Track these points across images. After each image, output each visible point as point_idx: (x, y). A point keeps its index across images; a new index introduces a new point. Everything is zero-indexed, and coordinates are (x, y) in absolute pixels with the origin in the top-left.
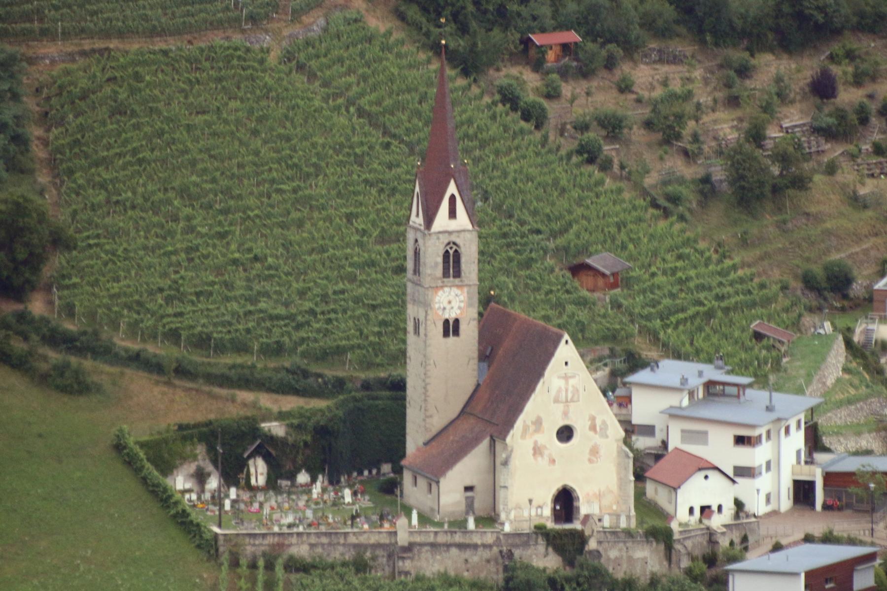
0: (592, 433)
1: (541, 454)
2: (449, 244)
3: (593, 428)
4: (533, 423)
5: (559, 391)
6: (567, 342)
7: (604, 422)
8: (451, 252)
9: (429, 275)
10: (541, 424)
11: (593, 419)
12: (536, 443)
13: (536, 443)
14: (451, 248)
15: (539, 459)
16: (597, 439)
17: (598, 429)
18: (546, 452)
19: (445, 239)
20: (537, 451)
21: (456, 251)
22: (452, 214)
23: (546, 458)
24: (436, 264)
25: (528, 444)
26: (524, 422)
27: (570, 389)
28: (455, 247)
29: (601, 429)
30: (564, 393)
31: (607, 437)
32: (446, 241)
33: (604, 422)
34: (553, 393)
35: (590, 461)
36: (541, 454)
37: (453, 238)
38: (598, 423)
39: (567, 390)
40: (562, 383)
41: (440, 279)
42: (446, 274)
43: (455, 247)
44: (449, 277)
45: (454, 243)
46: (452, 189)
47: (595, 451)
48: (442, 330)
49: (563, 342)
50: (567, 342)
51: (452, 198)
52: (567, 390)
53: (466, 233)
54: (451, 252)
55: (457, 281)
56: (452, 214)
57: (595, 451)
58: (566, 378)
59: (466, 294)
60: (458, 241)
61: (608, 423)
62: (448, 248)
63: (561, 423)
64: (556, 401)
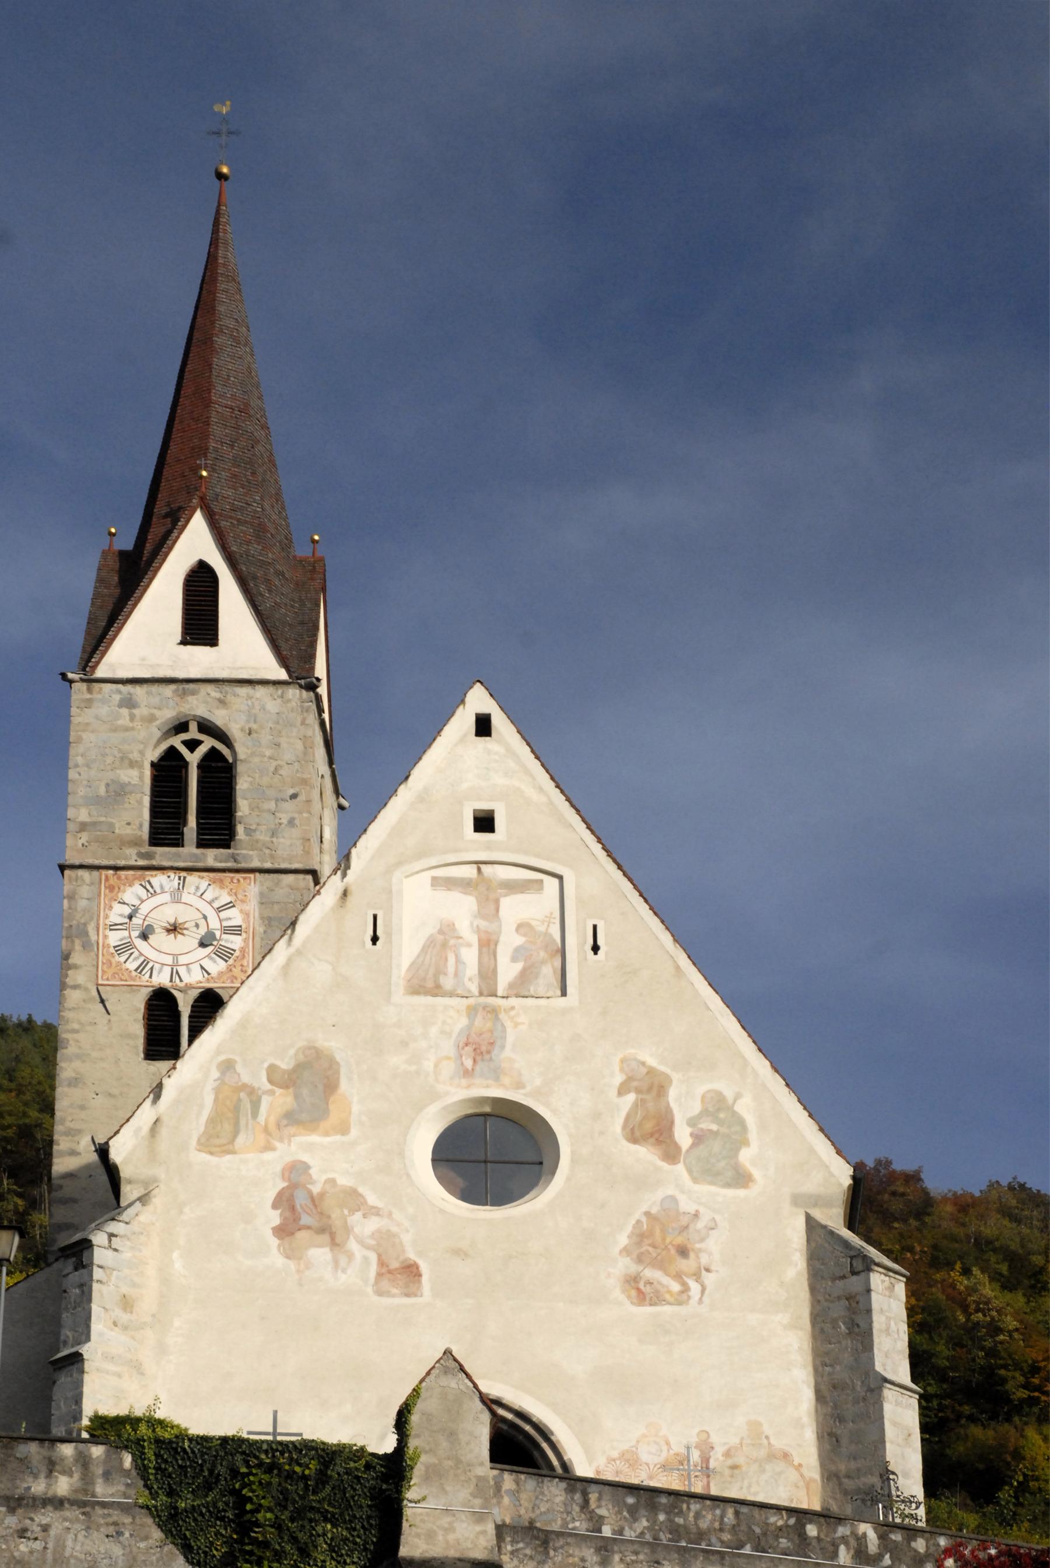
0: (645, 1154)
1: (331, 1235)
2: (182, 727)
3: (653, 1129)
4: (279, 1079)
5: (443, 941)
6: (483, 726)
7: (717, 1106)
8: (193, 759)
9: (83, 827)
10: (331, 1086)
11: (651, 1087)
12: (296, 1173)
13: (296, 1173)
14: (192, 745)
15: (320, 1254)
16: (681, 1187)
17: (683, 1136)
18: (364, 1227)
19: (167, 707)
20: (303, 1214)
21: (213, 754)
22: (200, 624)
23: (360, 1265)
24: (119, 792)
25: (254, 1173)
26: (228, 1066)
27: (509, 941)
28: (208, 743)
29: (698, 1138)
30: (470, 956)
31: (742, 1179)
32: (168, 714)
33: (717, 1106)
34: (407, 946)
35: (640, 1292)
36: (331, 1235)
37: (200, 705)
38: (684, 1105)
39: (488, 945)
40: (461, 909)
41: (135, 843)
42: (165, 829)
43: (208, 743)
44: (178, 842)
45: (207, 728)
46: (195, 542)
47: (664, 1250)
48: (138, 1030)
49: (463, 721)
50: (483, 726)
51: (200, 586)
52: (488, 945)
53: (261, 692)
54: (193, 759)
55: (211, 857)
56: (200, 624)
57: (664, 1250)
58: (486, 891)
59: (252, 906)
60: (219, 718)
61: (745, 1108)
62: (177, 741)
63: (453, 1096)
64: (426, 984)
